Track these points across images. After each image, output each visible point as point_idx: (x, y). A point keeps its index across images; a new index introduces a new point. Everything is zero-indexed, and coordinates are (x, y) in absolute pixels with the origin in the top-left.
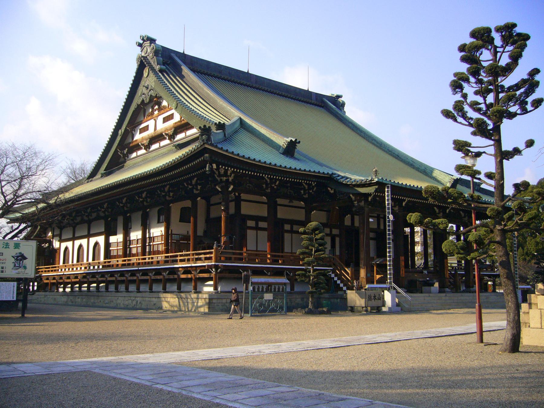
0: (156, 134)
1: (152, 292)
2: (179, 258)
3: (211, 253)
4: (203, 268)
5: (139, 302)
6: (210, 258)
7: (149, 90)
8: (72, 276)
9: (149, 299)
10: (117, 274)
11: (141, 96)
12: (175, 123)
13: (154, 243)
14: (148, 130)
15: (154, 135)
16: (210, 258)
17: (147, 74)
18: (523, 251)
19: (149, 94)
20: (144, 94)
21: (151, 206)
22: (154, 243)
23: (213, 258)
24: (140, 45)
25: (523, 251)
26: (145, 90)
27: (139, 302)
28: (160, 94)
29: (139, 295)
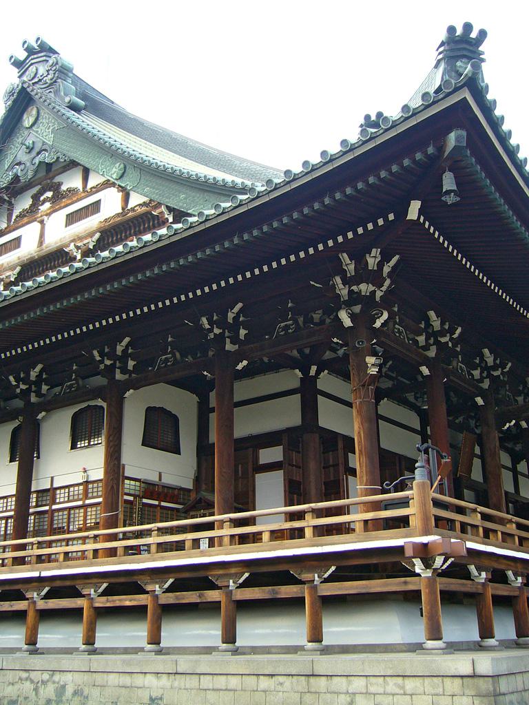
0: (43, 253)
1: (94, 652)
2: (153, 540)
3: (405, 503)
4: (58, 583)
5: (69, 690)
6: (403, 522)
7: (34, 153)
8: (204, 545)
9: (126, 680)
10: (39, 590)
11: (11, 168)
12: (106, 220)
13: (54, 507)
14: (18, 246)
15: (36, 255)
16: (403, 522)
17: (32, 120)
18: (442, 566)
19: (37, 161)
20: (19, 164)
21: (51, 405)
22: (54, 507)
23: (412, 521)
24: (18, 64)
25: (442, 566)
26: (23, 156)
27: (69, 690)
28: (69, 154)
29: (37, 661)
